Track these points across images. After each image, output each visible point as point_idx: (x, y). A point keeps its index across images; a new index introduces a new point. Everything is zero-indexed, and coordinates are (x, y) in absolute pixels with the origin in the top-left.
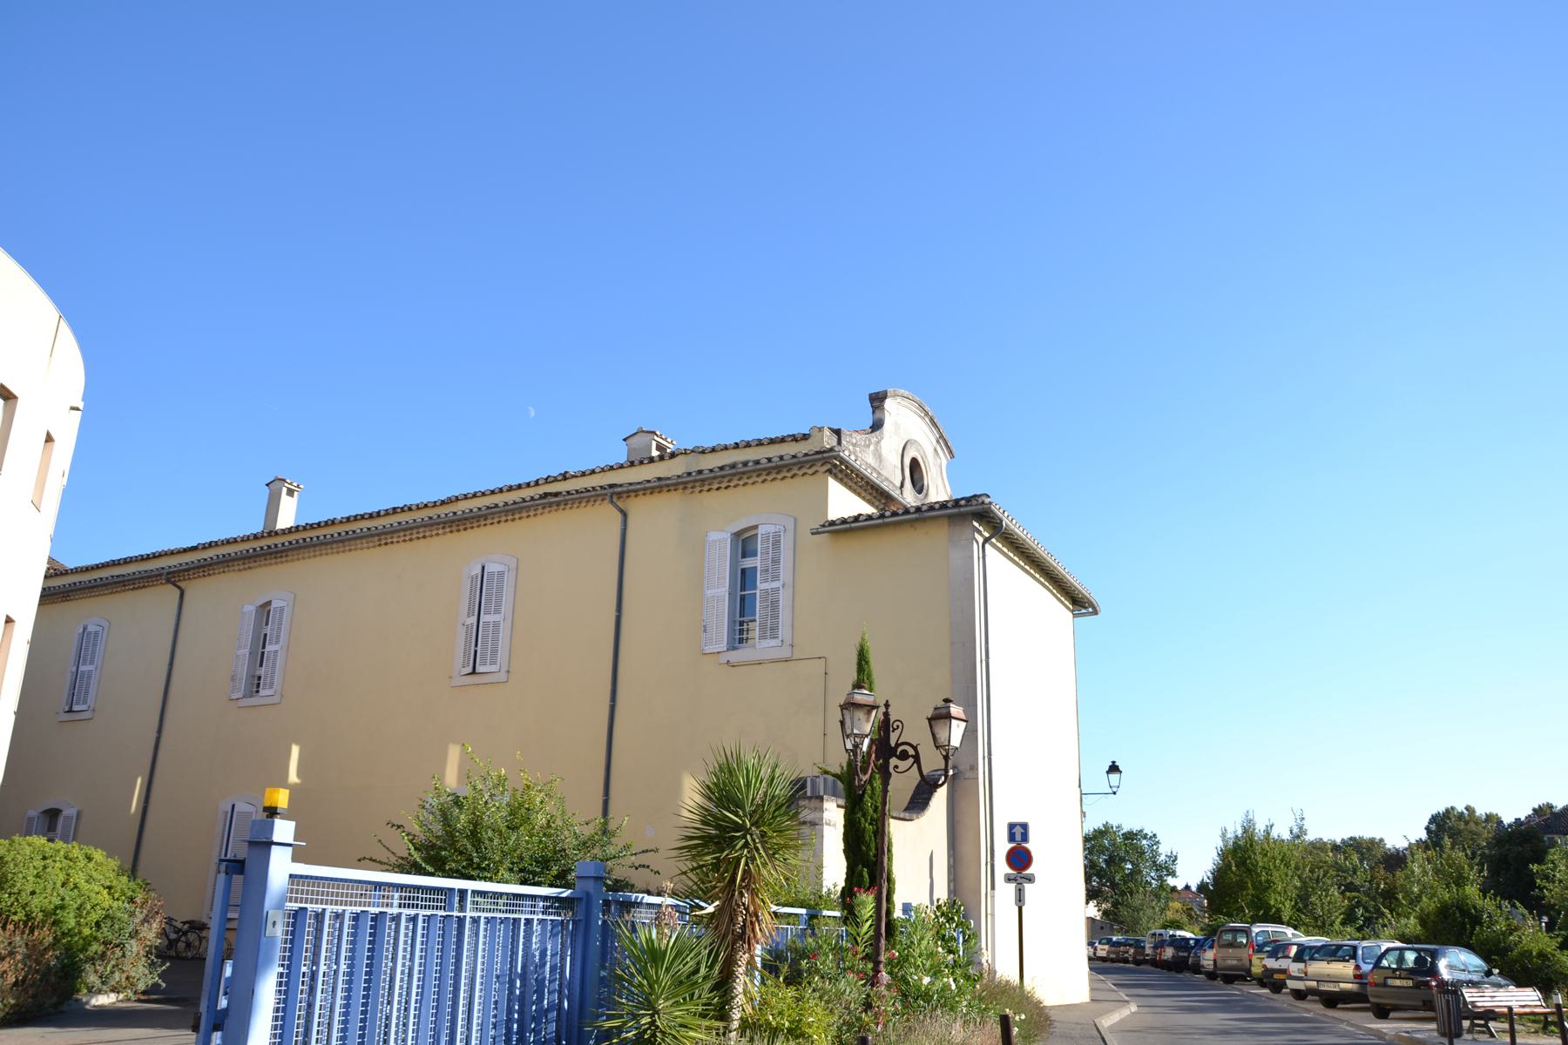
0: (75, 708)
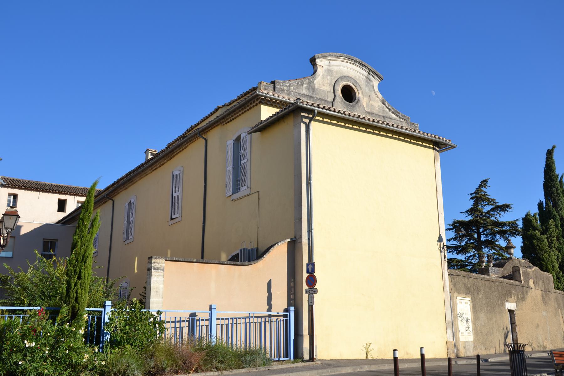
0: (174, 217)
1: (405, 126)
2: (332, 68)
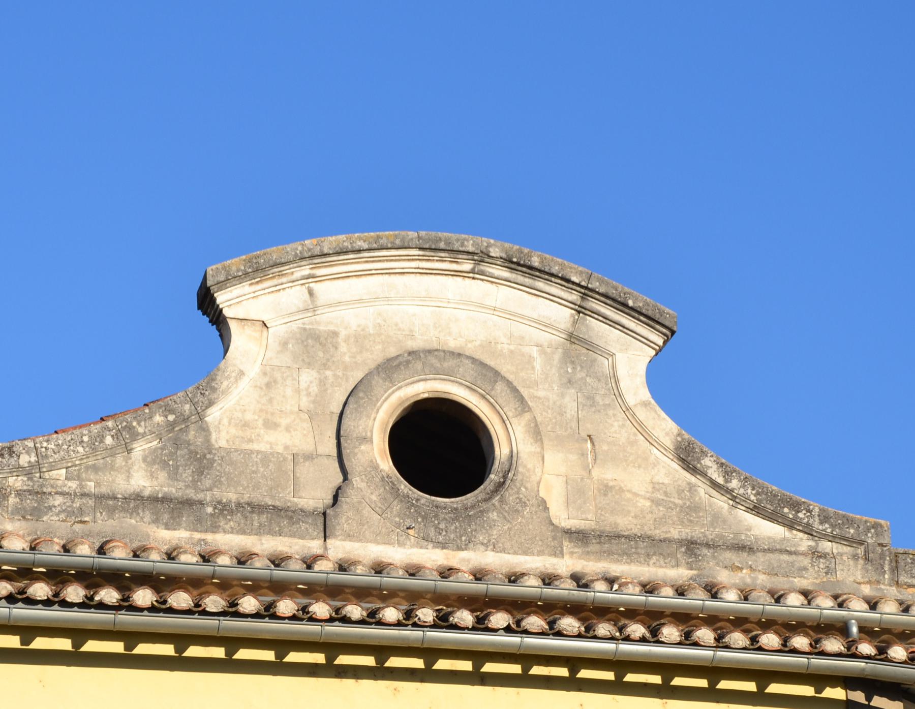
1: (851, 573)
2: (325, 320)
